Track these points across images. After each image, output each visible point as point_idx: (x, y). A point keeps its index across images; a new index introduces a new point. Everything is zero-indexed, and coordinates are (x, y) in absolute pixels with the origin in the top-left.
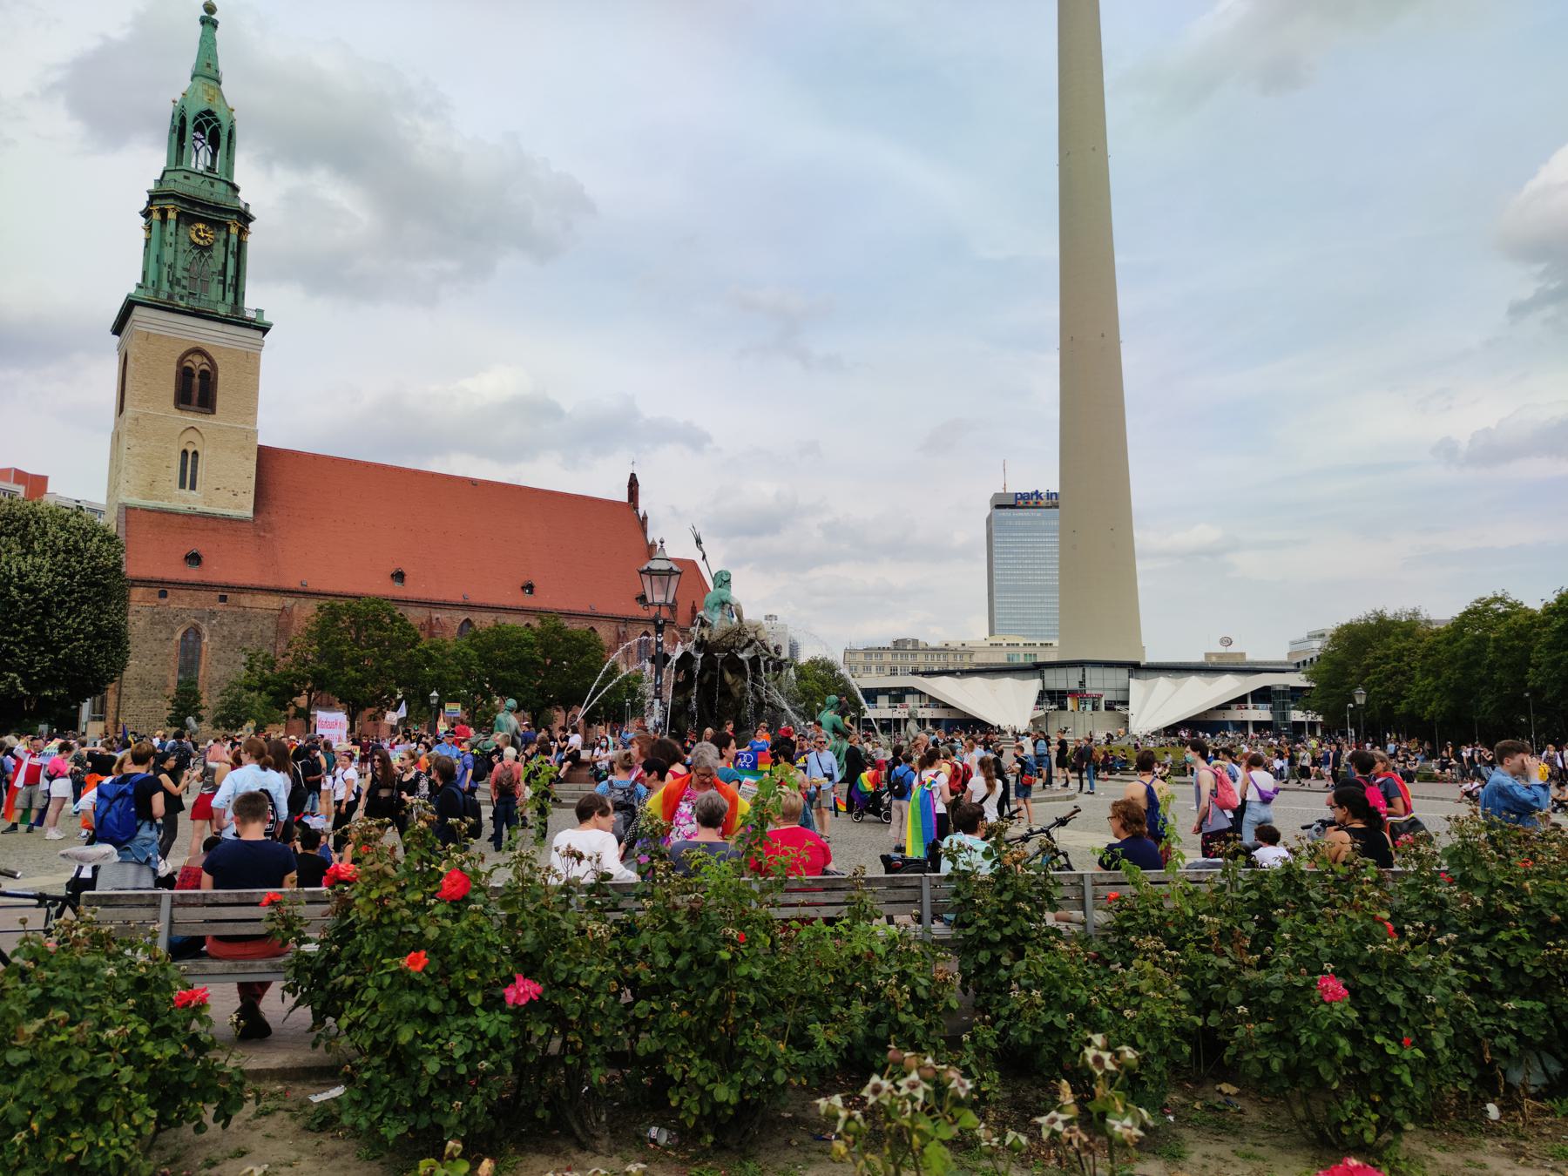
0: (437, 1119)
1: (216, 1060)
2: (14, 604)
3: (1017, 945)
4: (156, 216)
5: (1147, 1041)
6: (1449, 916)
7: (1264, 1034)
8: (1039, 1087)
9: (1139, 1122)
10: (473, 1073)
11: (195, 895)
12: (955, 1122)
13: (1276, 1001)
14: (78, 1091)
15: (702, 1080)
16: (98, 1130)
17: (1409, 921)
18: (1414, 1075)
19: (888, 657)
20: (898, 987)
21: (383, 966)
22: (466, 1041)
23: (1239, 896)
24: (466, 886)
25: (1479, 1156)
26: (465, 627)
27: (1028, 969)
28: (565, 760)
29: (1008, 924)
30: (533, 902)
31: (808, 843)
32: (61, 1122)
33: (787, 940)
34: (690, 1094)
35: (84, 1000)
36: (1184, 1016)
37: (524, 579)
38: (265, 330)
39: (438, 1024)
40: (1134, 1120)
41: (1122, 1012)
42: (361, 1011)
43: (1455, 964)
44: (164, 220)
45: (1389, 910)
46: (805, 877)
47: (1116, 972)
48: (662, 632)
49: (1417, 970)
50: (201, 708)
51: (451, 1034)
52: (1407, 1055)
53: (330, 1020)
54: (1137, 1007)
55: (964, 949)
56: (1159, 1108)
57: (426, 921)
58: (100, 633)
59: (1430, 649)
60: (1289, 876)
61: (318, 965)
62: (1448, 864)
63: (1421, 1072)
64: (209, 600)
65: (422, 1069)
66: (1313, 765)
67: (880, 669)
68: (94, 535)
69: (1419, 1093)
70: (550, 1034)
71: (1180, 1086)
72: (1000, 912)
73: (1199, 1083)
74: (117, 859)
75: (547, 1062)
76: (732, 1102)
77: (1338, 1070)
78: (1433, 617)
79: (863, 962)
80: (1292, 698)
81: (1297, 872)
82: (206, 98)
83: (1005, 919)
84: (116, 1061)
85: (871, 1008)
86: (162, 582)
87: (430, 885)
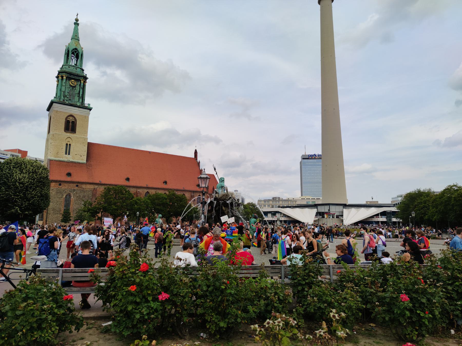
0: (139, 330)
1: (75, 314)
2: (17, 188)
3: (310, 285)
4: (60, 78)
5: (348, 312)
6: (440, 278)
7: (384, 310)
8: (316, 324)
9: (346, 333)
10: (149, 318)
11: (69, 270)
12: (291, 332)
13: (388, 301)
14: (36, 322)
15: (216, 321)
16: (42, 332)
17: (428, 279)
18: (429, 322)
19: (271, 202)
20: (274, 296)
21: (123, 289)
22: (147, 310)
23: (377, 272)
24: (147, 267)
25: (447, 344)
26: (147, 194)
27: (313, 292)
28: (176, 232)
29: (307, 279)
30: (167, 272)
31: (248, 256)
32: (32, 329)
33: (242, 283)
34: (213, 325)
35: (38, 298)
36: (360, 305)
37: (164, 180)
38: (90, 109)
39: (139, 305)
40: (344, 332)
41: (341, 304)
42: (117, 301)
43: (442, 291)
44: (62, 79)
45: (422, 276)
46: (247, 266)
47: (339, 293)
48: (204, 195)
49: (430, 293)
50: (71, 217)
51: (143, 308)
52: (427, 316)
53: (108, 304)
54: (346, 303)
55: (294, 286)
56: (352, 330)
57: (136, 277)
58: (42, 196)
59: (434, 200)
60: (392, 266)
61: (105, 289)
62: (440, 263)
63: (431, 321)
64: (73, 186)
65: (135, 317)
66: (399, 234)
67: (269, 206)
68: (41, 168)
69: (430, 327)
70: (172, 308)
71: (358, 324)
72: (305, 276)
73: (363, 323)
74: (47, 259)
75: (171, 316)
76: (225, 327)
77: (406, 320)
78: (435, 191)
79: (264, 289)
81: (395, 265)
82: (75, 45)
83: (306, 278)
84: (47, 314)
85: (266, 302)
86: (60, 181)
87: (137, 267)
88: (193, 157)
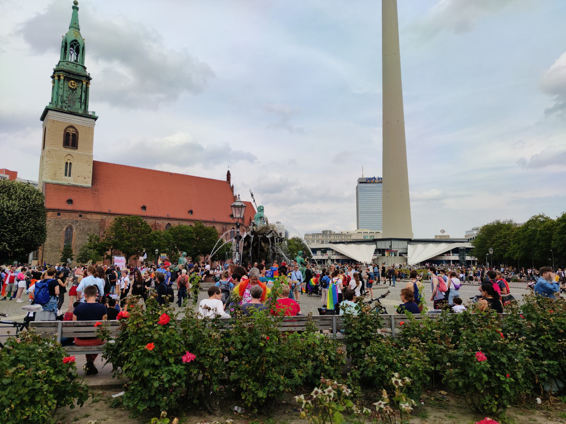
0: (158, 403)
1: (78, 382)
2: (5, 218)
3: (367, 341)
4: (56, 78)
5: (414, 375)
6: (523, 330)
7: (456, 373)
8: (375, 392)
9: (411, 405)
10: (171, 387)
11: (70, 323)
12: (345, 405)
13: (461, 361)
14: (28, 393)
15: (253, 389)
16: (35, 407)
17: (508, 332)
18: (510, 388)
19: (320, 237)
20: (324, 356)
21: (138, 348)
22: (168, 375)
23: (447, 323)
24: (168, 319)
25: (534, 417)
26: (168, 226)
27: (371, 349)
28: (204, 274)
29: (364, 333)
30: (192, 325)
31: (292, 304)
32: (22, 405)
33: (284, 339)
34: (249, 395)
35: (30, 361)
36: (428, 366)
37: (189, 209)
38: (96, 119)
39: (158, 369)
40: (409, 404)
41: (405, 365)
42: (130, 365)
43: (525, 348)
44: (59, 79)
45: (502, 328)
46: (291, 316)
47: (403, 351)
48: (239, 228)
49: (512, 350)
50: (72, 255)
51: (163, 373)
52: (508, 380)
53: (119, 368)
54: (410, 363)
55: (348, 342)
56: (418, 399)
57: (154, 332)
58: (36, 228)
59: (516, 234)
60: (465, 316)
61: (115, 348)
62: (523, 311)
63: (513, 386)
64: (75, 216)
65: (152, 385)
66: (474, 276)
67: (318, 241)
68: (34, 193)
69: (512, 394)
70: (198, 373)
71: (426, 391)
72: (361, 329)
73: (433, 390)
74: (42, 310)
75: (197, 383)
76: (264, 397)
77: (483, 386)
78: (517, 223)
79: (311, 347)
80: (466, 252)
81: (468, 314)
82: (74, 35)
83: (363, 331)
84: (42, 383)
85: (314, 363)
86: (59, 210)
87: (155, 319)
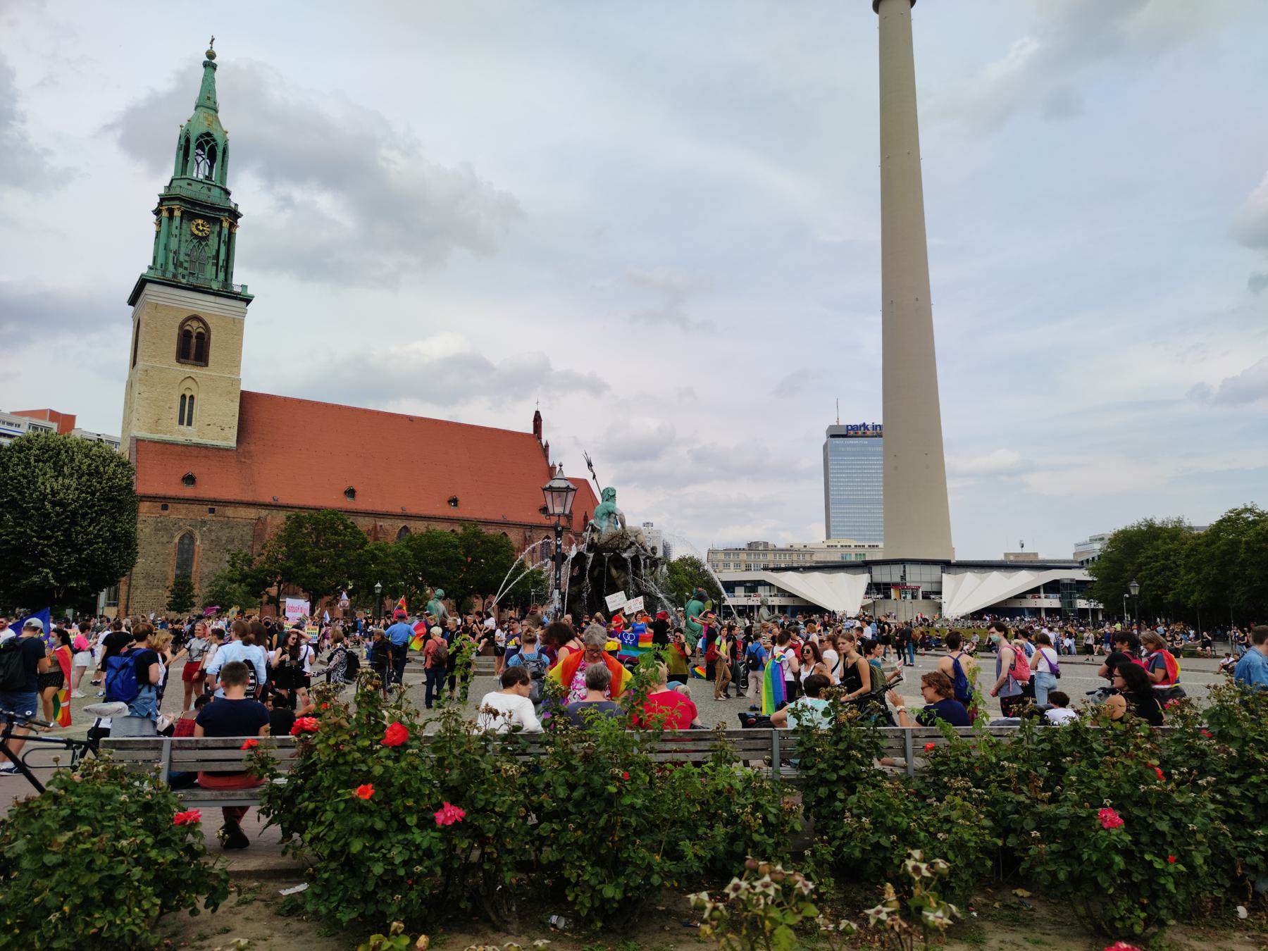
0: (381, 907)
1: (206, 863)
2: (48, 515)
3: (850, 784)
4: (165, 214)
5: (956, 857)
6: (1208, 764)
7: (1053, 852)
8: (866, 889)
9: (948, 915)
10: (410, 874)
11: (190, 741)
12: (800, 912)
13: (1064, 828)
14: (99, 884)
15: (593, 882)
16: (116, 914)
17: (1174, 767)
18: (1177, 884)
19: (743, 556)
20: (752, 814)
21: (339, 795)
22: (404, 851)
23: (1034, 747)
24: (405, 735)
25: (1228, 944)
26: (403, 533)
27: (859, 801)
28: (483, 638)
29: (843, 767)
30: (458, 747)
31: (680, 704)
32: (87, 906)
33: (663, 778)
34: (583, 892)
35: (103, 819)
36: (988, 838)
37: (450, 494)
38: (248, 301)
39: (382, 839)
40: (945, 912)
41: (936, 835)
42: (321, 829)
43: (1213, 800)
44: (171, 217)
45: (1159, 758)
46: (677, 730)
47: (931, 805)
48: (560, 537)
49: (1181, 805)
50: (194, 596)
51: (393, 846)
52: (1171, 869)
53: (296, 835)
54: (949, 831)
55: (806, 786)
56: (965, 906)
57: (373, 762)
58: (115, 538)
59: (1192, 550)
60: (1076, 731)
61: (287, 794)
62: (1208, 723)
63: (1183, 881)
64: (200, 512)
65: (369, 871)
66: (1096, 644)
67: (737, 566)
68: (111, 462)
69: (1180, 898)
70: (471, 847)
71: (982, 890)
72: (836, 758)
73: (998, 888)
74: (128, 713)
75: (468, 868)
76: (617, 898)
77: (1114, 879)
78: (1194, 524)
79: (725, 796)
81: (1083, 729)
82: (206, 123)
83: (841, 764)
84: (128, 863)
85: (729, 829)
86: (165, 498)
87: (376, 734)
88: (531, 431)
